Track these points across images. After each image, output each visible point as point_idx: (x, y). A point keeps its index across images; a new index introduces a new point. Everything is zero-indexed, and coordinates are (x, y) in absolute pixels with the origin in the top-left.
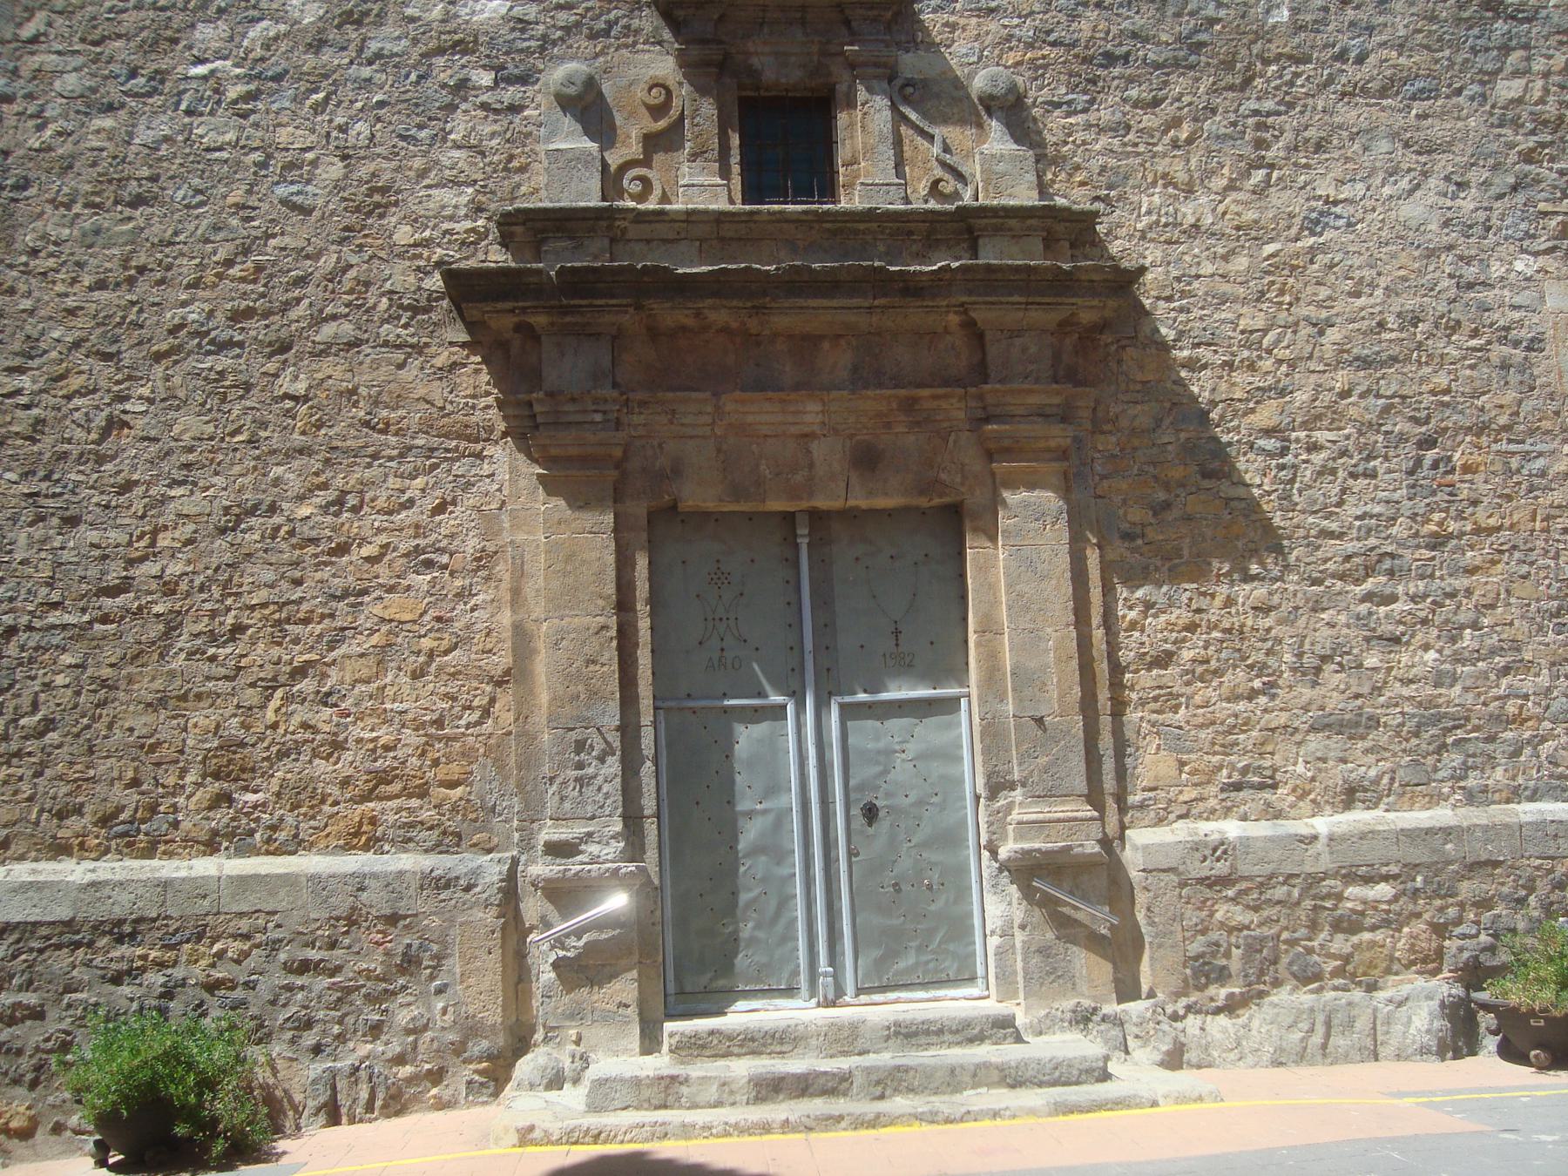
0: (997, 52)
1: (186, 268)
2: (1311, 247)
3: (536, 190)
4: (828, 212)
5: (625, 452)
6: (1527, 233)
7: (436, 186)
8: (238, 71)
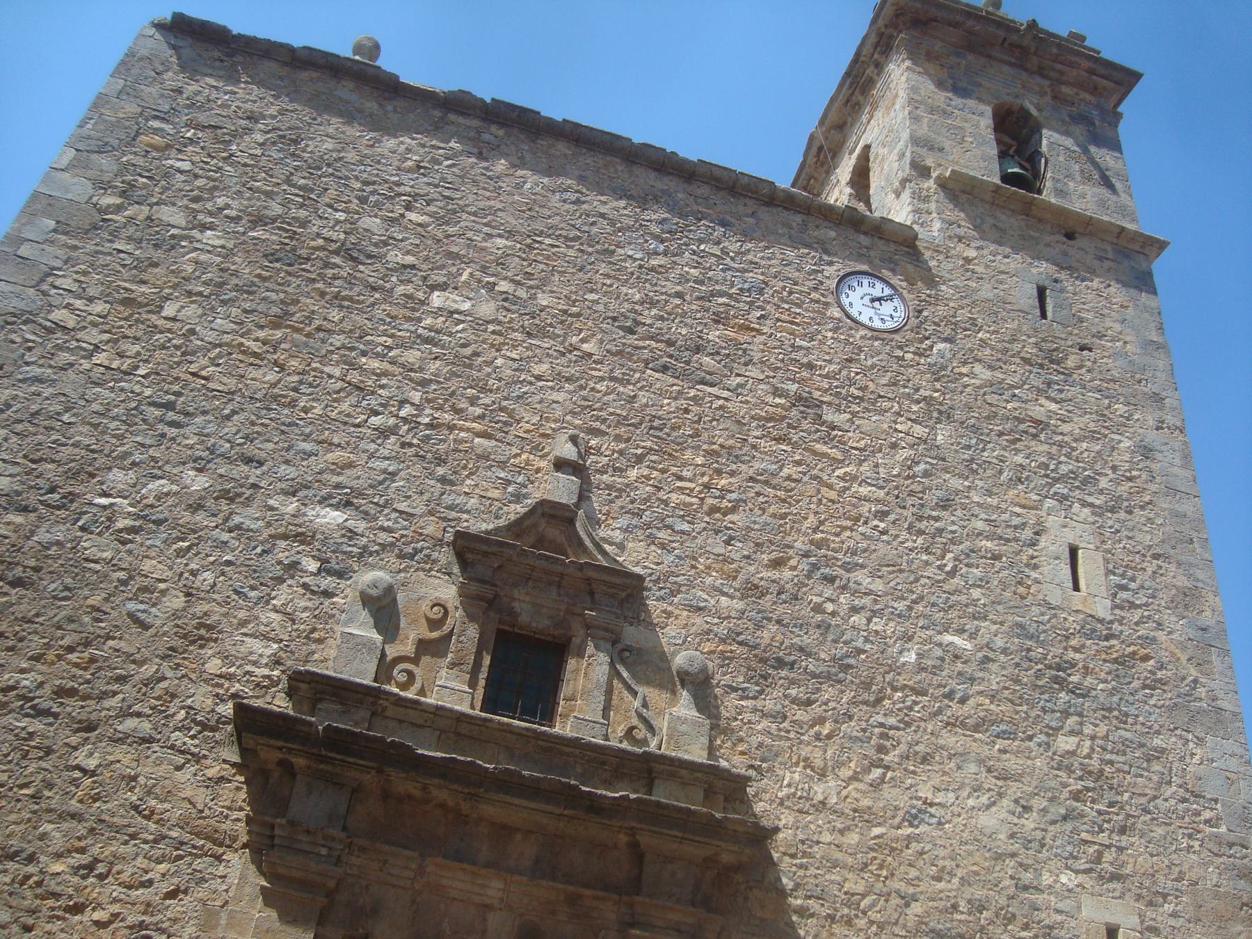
0: (697, 640)
1: (36, 644)
2: (909, 836)
3: (326, 660)
4: (544, 733)
5: (337, 885)
6: (1071, 854)
7: (251, 635)
8: (131, 509)
